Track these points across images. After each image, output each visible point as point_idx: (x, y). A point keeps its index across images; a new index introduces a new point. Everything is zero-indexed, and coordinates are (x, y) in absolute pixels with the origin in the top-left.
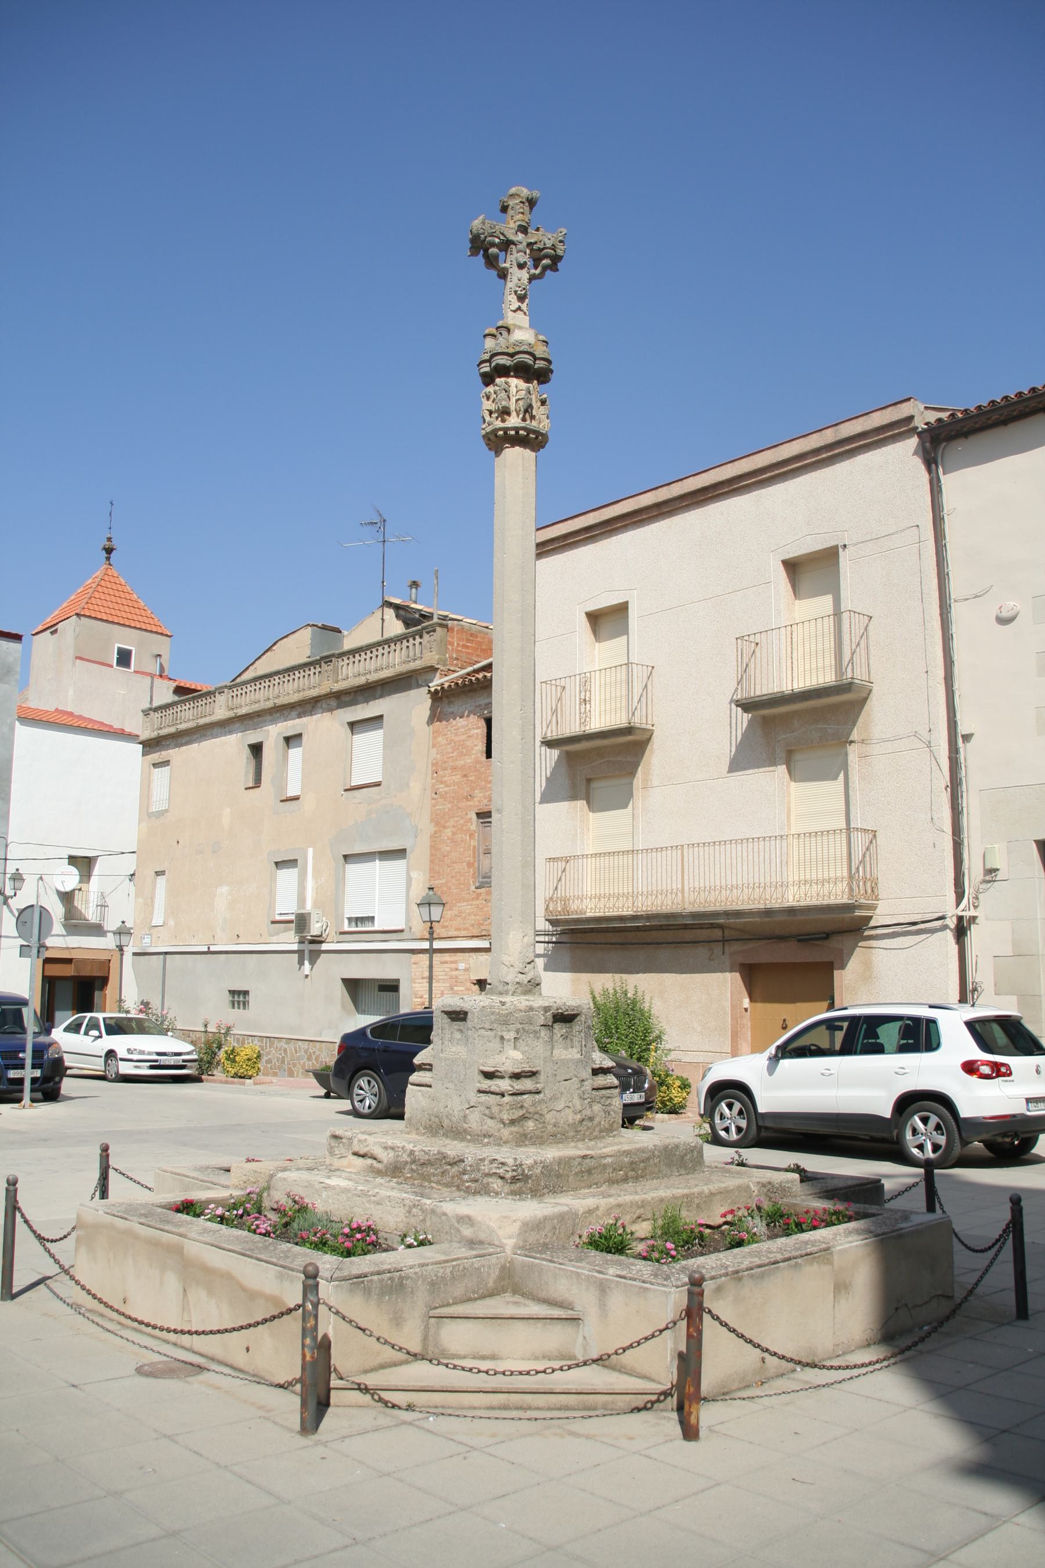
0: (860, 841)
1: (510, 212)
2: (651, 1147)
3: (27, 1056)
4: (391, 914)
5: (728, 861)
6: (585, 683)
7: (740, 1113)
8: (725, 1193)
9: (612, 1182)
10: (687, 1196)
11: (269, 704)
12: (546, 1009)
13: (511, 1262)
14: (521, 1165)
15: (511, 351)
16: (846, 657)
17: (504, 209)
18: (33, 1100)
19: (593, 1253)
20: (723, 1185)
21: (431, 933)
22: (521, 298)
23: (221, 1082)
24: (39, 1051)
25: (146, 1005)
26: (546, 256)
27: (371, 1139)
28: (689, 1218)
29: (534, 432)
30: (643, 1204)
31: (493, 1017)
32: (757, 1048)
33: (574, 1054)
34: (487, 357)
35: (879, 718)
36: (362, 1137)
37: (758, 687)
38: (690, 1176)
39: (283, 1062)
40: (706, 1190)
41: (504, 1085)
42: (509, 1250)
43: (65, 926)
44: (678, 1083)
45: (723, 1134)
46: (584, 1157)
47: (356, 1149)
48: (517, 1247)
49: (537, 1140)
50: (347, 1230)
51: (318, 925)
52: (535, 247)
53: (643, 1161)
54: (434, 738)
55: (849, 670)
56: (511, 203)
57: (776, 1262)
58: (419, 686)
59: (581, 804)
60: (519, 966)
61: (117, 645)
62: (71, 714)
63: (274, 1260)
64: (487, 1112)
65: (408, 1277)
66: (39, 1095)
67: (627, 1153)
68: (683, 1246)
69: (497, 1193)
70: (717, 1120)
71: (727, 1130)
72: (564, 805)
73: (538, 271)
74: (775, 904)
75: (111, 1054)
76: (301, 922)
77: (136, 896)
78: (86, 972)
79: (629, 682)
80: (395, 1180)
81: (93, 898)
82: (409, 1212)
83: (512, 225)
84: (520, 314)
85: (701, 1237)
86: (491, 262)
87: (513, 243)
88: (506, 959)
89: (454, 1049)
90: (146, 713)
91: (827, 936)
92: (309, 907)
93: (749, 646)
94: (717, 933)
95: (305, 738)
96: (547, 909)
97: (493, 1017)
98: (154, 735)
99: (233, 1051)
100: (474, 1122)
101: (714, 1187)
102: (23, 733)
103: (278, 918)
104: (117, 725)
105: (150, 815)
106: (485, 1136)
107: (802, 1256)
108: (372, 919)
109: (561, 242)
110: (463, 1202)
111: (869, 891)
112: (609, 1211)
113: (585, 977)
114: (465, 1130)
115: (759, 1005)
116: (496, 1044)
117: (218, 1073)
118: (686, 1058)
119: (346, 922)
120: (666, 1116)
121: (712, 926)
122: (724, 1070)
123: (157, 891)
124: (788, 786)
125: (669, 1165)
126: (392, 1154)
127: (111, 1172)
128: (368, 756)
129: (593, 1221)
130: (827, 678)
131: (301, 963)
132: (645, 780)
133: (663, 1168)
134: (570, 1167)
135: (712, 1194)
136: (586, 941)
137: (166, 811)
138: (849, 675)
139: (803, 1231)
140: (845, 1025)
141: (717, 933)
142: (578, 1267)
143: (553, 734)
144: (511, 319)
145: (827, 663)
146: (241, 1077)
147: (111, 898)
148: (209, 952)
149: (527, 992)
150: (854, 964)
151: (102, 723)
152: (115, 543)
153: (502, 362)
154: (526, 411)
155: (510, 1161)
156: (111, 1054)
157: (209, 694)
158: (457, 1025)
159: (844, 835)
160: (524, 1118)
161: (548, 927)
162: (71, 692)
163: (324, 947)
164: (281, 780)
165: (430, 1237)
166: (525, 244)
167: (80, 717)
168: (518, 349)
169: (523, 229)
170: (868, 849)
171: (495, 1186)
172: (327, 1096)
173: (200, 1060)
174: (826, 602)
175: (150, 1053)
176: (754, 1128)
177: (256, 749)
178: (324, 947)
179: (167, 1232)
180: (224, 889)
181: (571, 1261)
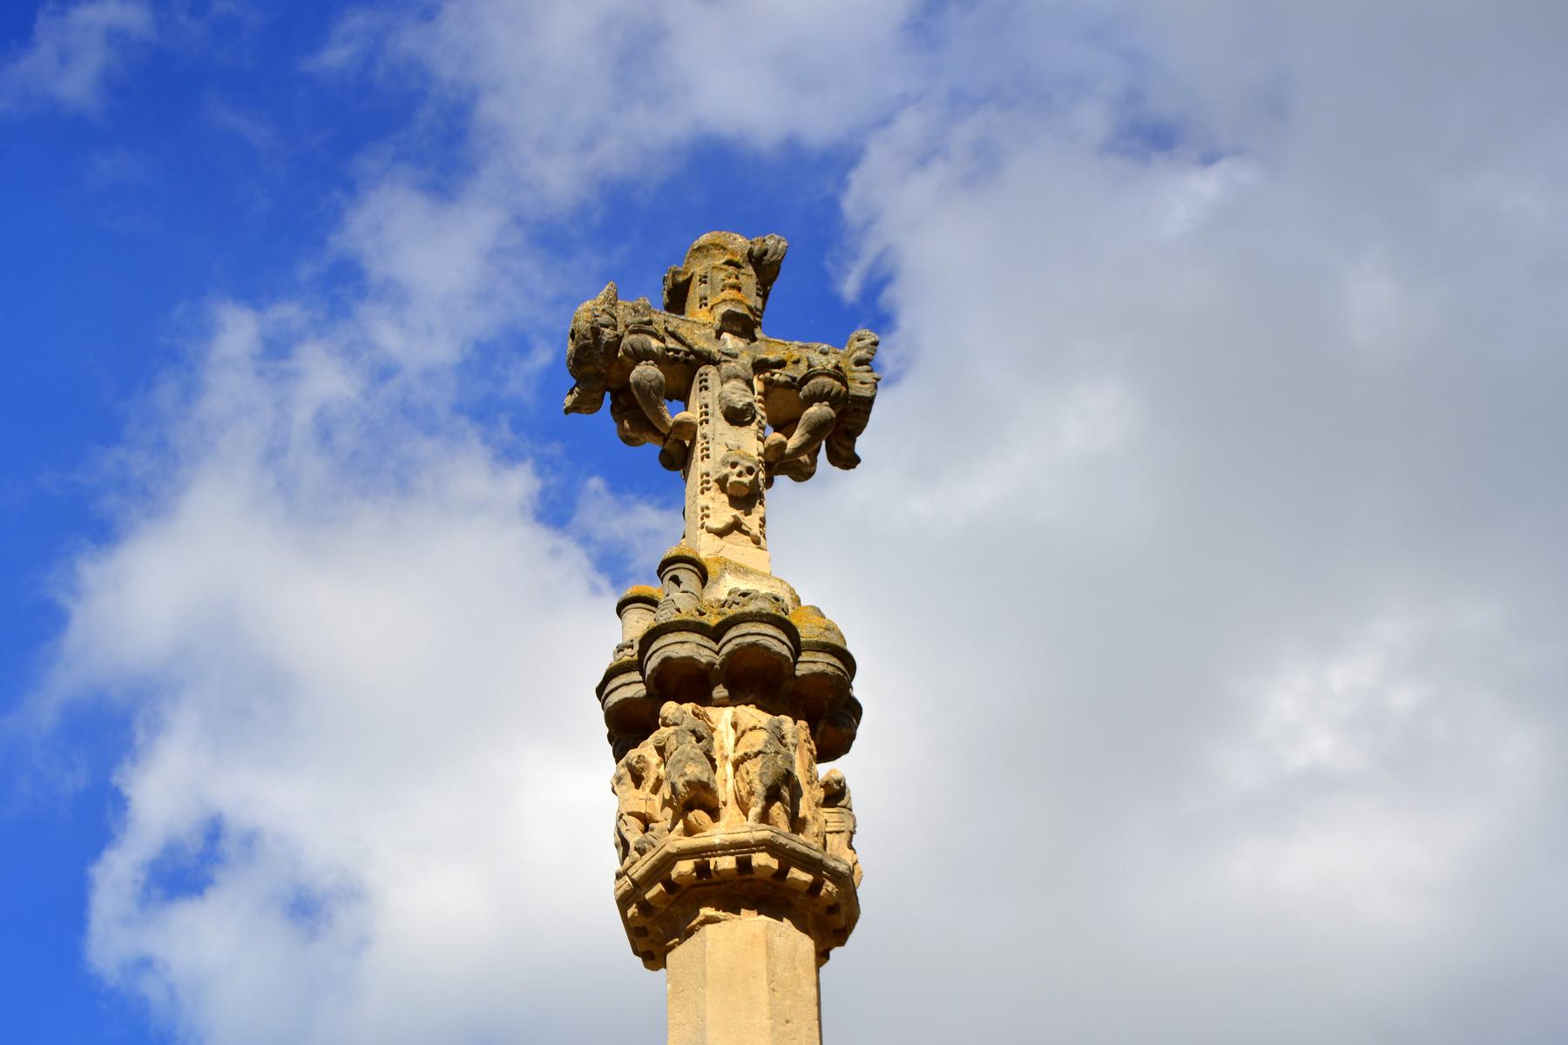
15: (713, 620)
29: (808, 863)
52: (779, 376)
56: (698, 269)
73: (793, 442)
87: (707, 359)
109: (859, 362)
154: (772, 796)
166: (746, 360)
169: (741, 325)
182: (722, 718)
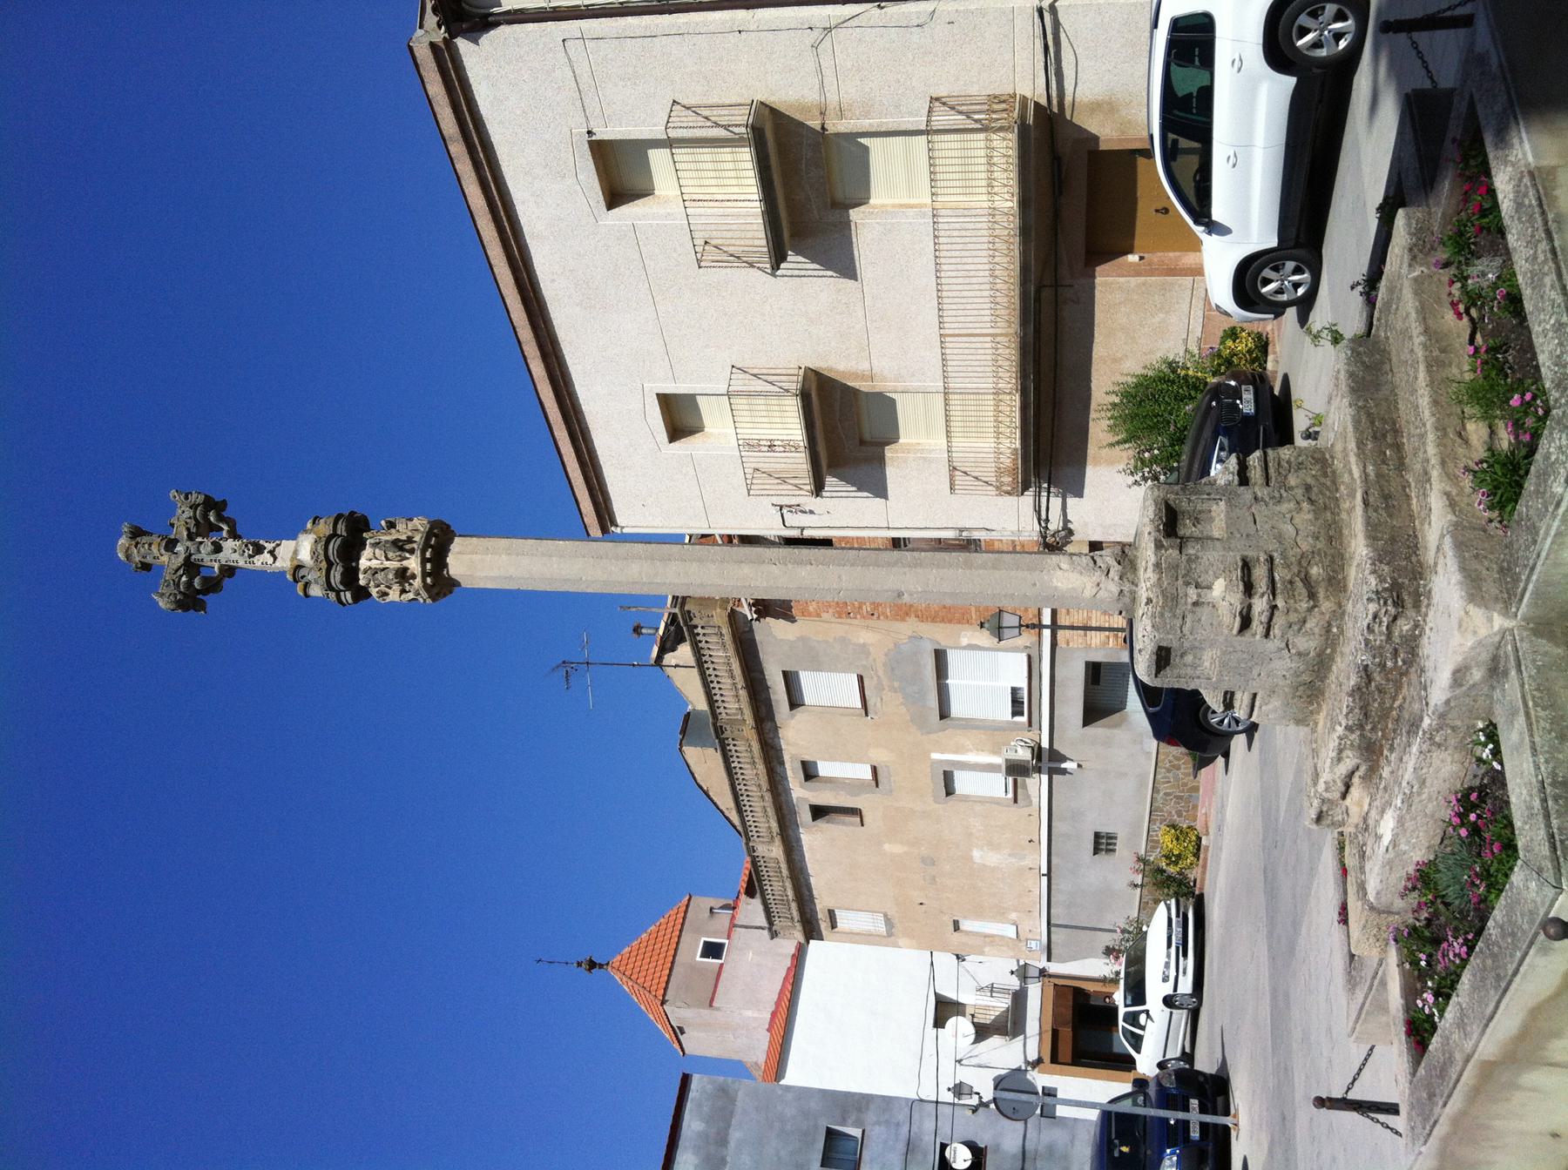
0: (943, 118)
1: (149, 560)
2: (1351, 411)
3: (1173, 1116)
4: (1010, 668)
5: (960, 280)
6: (750, 445)
7: (1276, 269)
8: (1424, 313)
9: (1401, 466)
10: (1429, 367)
11: (768, 796)
12: (1159, 546)
13: (1526, 619)
14: (1377, 592)
15: (324, 565)
16: (722, 133)
17: (146, 567)
18: (1227, 1113)
19: (1521, 508)
20: (1414, 315)
21: (1034, 626)
22: (259, 550)
23: (1204, 873)
24: (1167, 1100)
25: (1109, 951)
26: (205, 516)
27: (1325, 777)
28: (1463, 368)
29: (427, 539)
30: (1441, 429)
31: (1167, 614)
32: (1196, 245)
33: (1219, 510)
34: (332, 595)
35: (792, 91)
36: (1321, 786)
37: (757, 242)
38: (1394, 359)
39: (1181, 798)
40: (1418, 340)
41: (1260, 605)
42: (1509, 624)
43: (1015, 1035)
44: (1229, 343)
45: (1301, 291)
46: (1366, 503)
47: (1337, 795)
48: (1506, 613)
49: (1337, 562)
50: (1463, 832)
51: (1020, 750)
52: (194, 530)
53: (1372, 423)
54: (810, 615)
55: (736, 130)
57: (1553, 251)
58: (751, 630)
59: (889, 452)
60: (1097, 576)
61: (698, 959)
62: (774, 1014)
63: (1519, 954)
64: (1296, 628)
65: (1554, 774)
66: (1220, 1100)
67: (1360, 444)
68: (1506, 376)
69: (1416, 626)
70: (1284, 297)
71: (1296, 285)
72: (891, 472)
73: (225, 528)
74: (1014, 223)
75: (1168, 1001)
76: (1016, 770)
77: (982, 953)
78: (1069, 1014)
79: (749, 395)
80: (1386, 752)
81: (985, 1000)
82: (1439, 746)
83: (165, 559)
84: (280, 552)
85: (1492, 350)
86: (212, 585)
87: (188, 558)
88: (1088, 593)
89: (1207, 664)
90: (774, 935)
91: (1056, 159)
92: (998, 760)
93: (710, 252)
94: (1047, 294)
95: (807, 758)
96: (1009, 493)
97: (1167, 614)
98: (799, 926)
99: (1167, 857)
100: (1307, 643)
101: (1416, 329)
102: (795, 1075)
103: (1010, 795)
104: (788, 963)
105: (890, 934)
106: (1328, 631)
107: (1543, 213)
108: (1014, 691)
110: (1430, 674)
111: (1003, 106)
112: (1450, 477)
113: (1092, 450)
114: (1319, 655)
115: (1137, 242)
116: (1204, 612)
117: (1192, 875)
118: (1197, 331)
119: (1017, 719)
120: (1270, 358)
121: (1038, 299)
122: (1221, 289)
123: (976, 929)
124: (874, 207)
125: (1377, 386)
126: (1348, 753)
127: (1351, 1096)
128: (828, 689)
129: (1466, 500)
130: (745, 157)
131: (1064, 772)
132: (863, 377)
133: (1381, 395)
134: (1380, 523)
135: (1426, 331)
136: (1050, 451)
137: (885, 916)
138: (743, 130)
139: (1495, 206)
140: (1171, 136)
141: (1047, 294)
142: (1547, 533)
143: (807, 482)
144: (284, 563)
145: (729, 157)
146: (1199, 849)
147: (983, 980)
148: (1049, 875)
149: (1133, 566)
150: (1092, 125)
151: (786, 979)
152: (584, 957)
153: (338, 577)
154: (401, 549)
155: (1372, 607)
156: (1168, 1001)
157: (754, 862)
158: (1175, 660)
159: (936, 138)
160: (1306, 580)
161: (1030, 493)
162: (749, 1013)
163: (1045, 744)
164: (854, 786)
165: (1480, 725)
166: (189, 544)
167: (778, 1004)
168: (322, 557)
169: (171, 545)
170: (952, 108)
171: (1405, 628)
172: (1226, 755)
173: (1177, 896)
174: (658, 158)
175: (1169, 956)
176: (1296, 252)
177: (819, 812)
178: (1045, 744)
179: (1460, 1075)
180: (976, 854)
181: (1535, 542)
182: (364, 563)
